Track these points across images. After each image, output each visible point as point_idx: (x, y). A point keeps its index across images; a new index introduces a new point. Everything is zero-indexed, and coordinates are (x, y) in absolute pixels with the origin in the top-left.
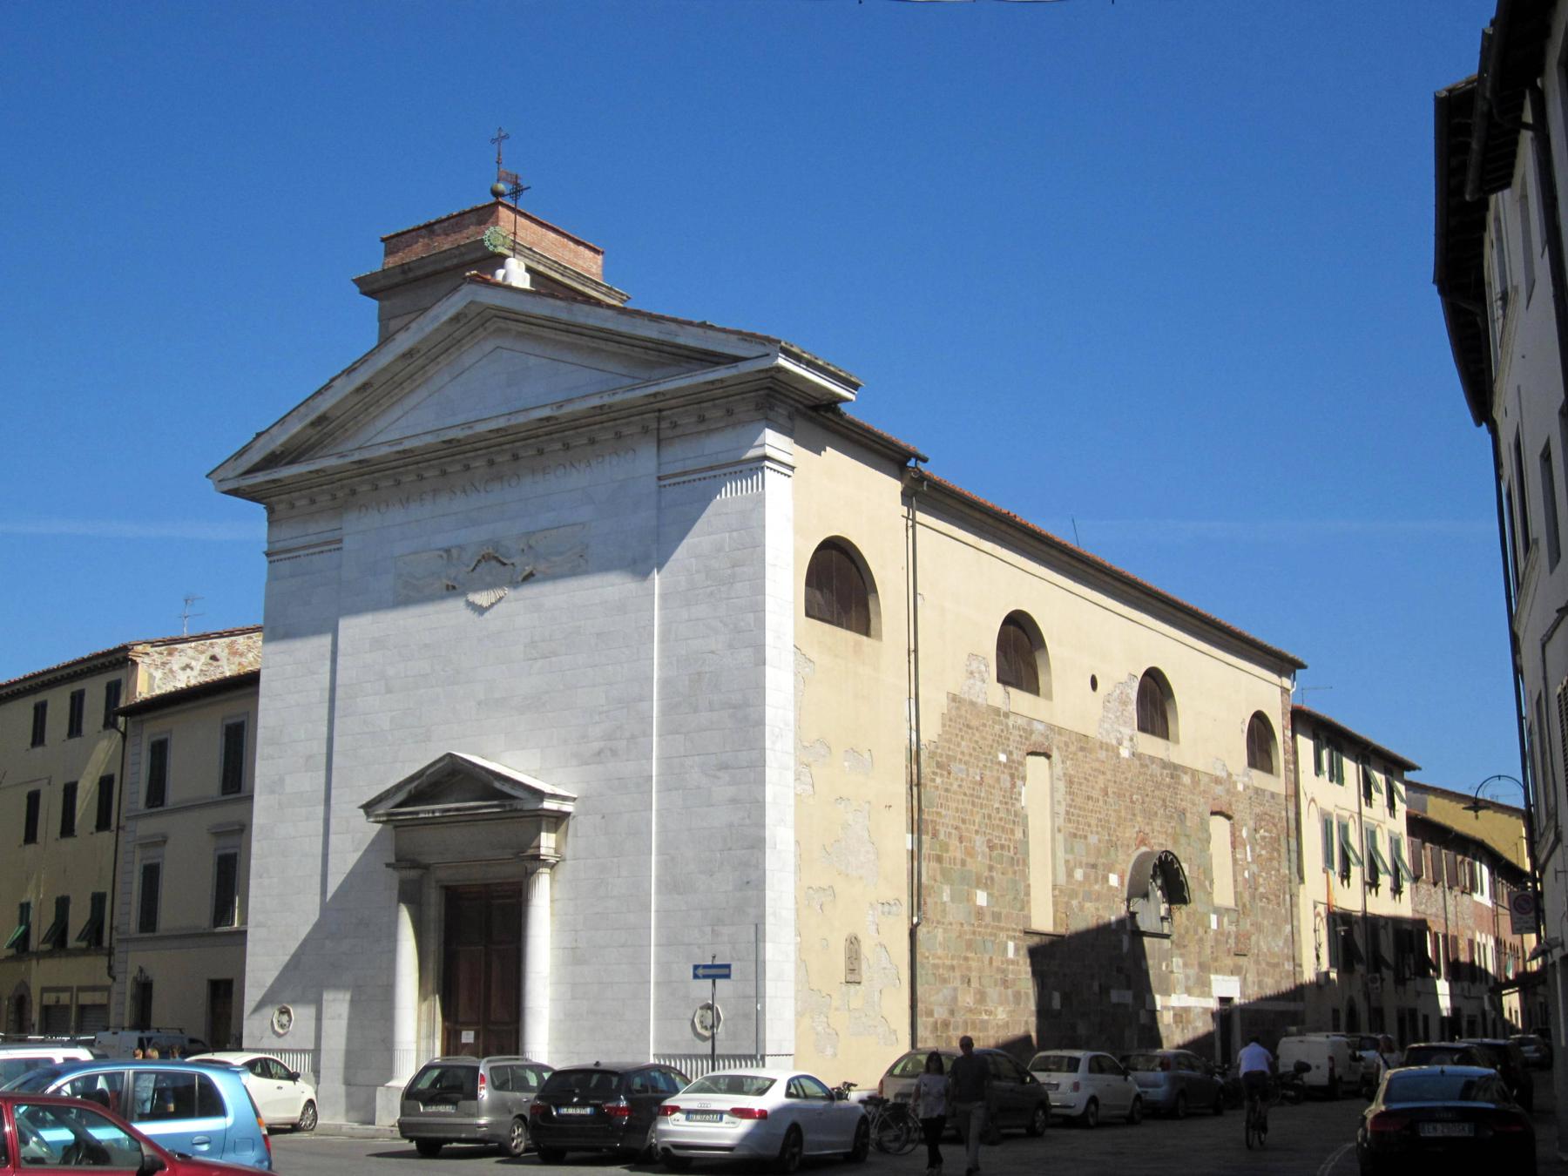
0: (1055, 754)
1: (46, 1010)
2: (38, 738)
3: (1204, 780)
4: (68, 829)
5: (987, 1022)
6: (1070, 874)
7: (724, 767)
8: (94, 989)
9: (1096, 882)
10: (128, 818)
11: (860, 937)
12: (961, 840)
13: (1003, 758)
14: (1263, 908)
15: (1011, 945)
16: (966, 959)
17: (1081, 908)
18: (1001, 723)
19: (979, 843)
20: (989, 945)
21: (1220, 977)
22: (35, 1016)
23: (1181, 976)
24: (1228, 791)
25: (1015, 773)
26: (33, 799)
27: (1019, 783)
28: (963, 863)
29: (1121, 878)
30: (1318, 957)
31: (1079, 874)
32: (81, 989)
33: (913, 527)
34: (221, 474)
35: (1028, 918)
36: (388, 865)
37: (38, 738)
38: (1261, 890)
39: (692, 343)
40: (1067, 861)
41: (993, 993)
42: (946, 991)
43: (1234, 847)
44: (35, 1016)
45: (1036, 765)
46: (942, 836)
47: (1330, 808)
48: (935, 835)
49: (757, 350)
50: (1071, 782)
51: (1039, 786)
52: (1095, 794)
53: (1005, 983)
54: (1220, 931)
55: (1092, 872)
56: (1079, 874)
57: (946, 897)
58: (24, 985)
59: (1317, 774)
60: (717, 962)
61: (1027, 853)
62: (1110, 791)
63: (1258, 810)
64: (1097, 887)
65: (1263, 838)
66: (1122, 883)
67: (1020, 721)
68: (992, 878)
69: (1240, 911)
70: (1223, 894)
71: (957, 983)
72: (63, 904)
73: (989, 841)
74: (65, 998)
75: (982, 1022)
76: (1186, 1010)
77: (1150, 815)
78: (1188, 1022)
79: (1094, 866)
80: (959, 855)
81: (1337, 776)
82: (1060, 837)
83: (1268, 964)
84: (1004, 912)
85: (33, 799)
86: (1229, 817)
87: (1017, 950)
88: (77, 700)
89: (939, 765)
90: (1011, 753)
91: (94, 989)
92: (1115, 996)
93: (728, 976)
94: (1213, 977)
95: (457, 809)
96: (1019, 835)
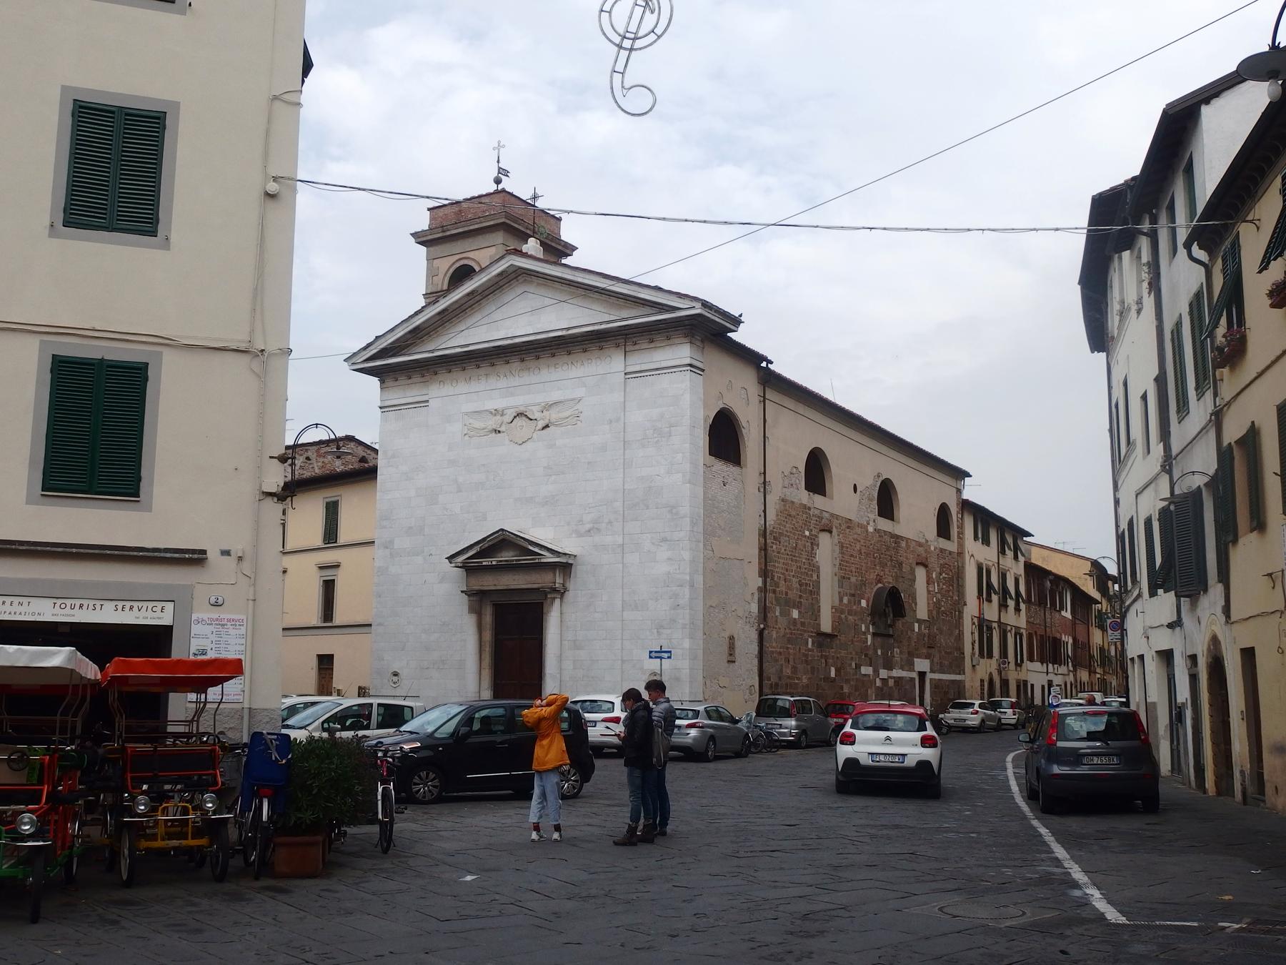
0: (834, 530)
7: (664, 540)
13: (807, 533)
25: (814, 543)
31: (845, 600)
45: (824, 539)
51: (826, 552)
56: (845, 600)
70: (922, 612)
77: (883, 565)
79: (853, 595)
81: (986, 542)
86: (926, 566)
96: (815, 577)
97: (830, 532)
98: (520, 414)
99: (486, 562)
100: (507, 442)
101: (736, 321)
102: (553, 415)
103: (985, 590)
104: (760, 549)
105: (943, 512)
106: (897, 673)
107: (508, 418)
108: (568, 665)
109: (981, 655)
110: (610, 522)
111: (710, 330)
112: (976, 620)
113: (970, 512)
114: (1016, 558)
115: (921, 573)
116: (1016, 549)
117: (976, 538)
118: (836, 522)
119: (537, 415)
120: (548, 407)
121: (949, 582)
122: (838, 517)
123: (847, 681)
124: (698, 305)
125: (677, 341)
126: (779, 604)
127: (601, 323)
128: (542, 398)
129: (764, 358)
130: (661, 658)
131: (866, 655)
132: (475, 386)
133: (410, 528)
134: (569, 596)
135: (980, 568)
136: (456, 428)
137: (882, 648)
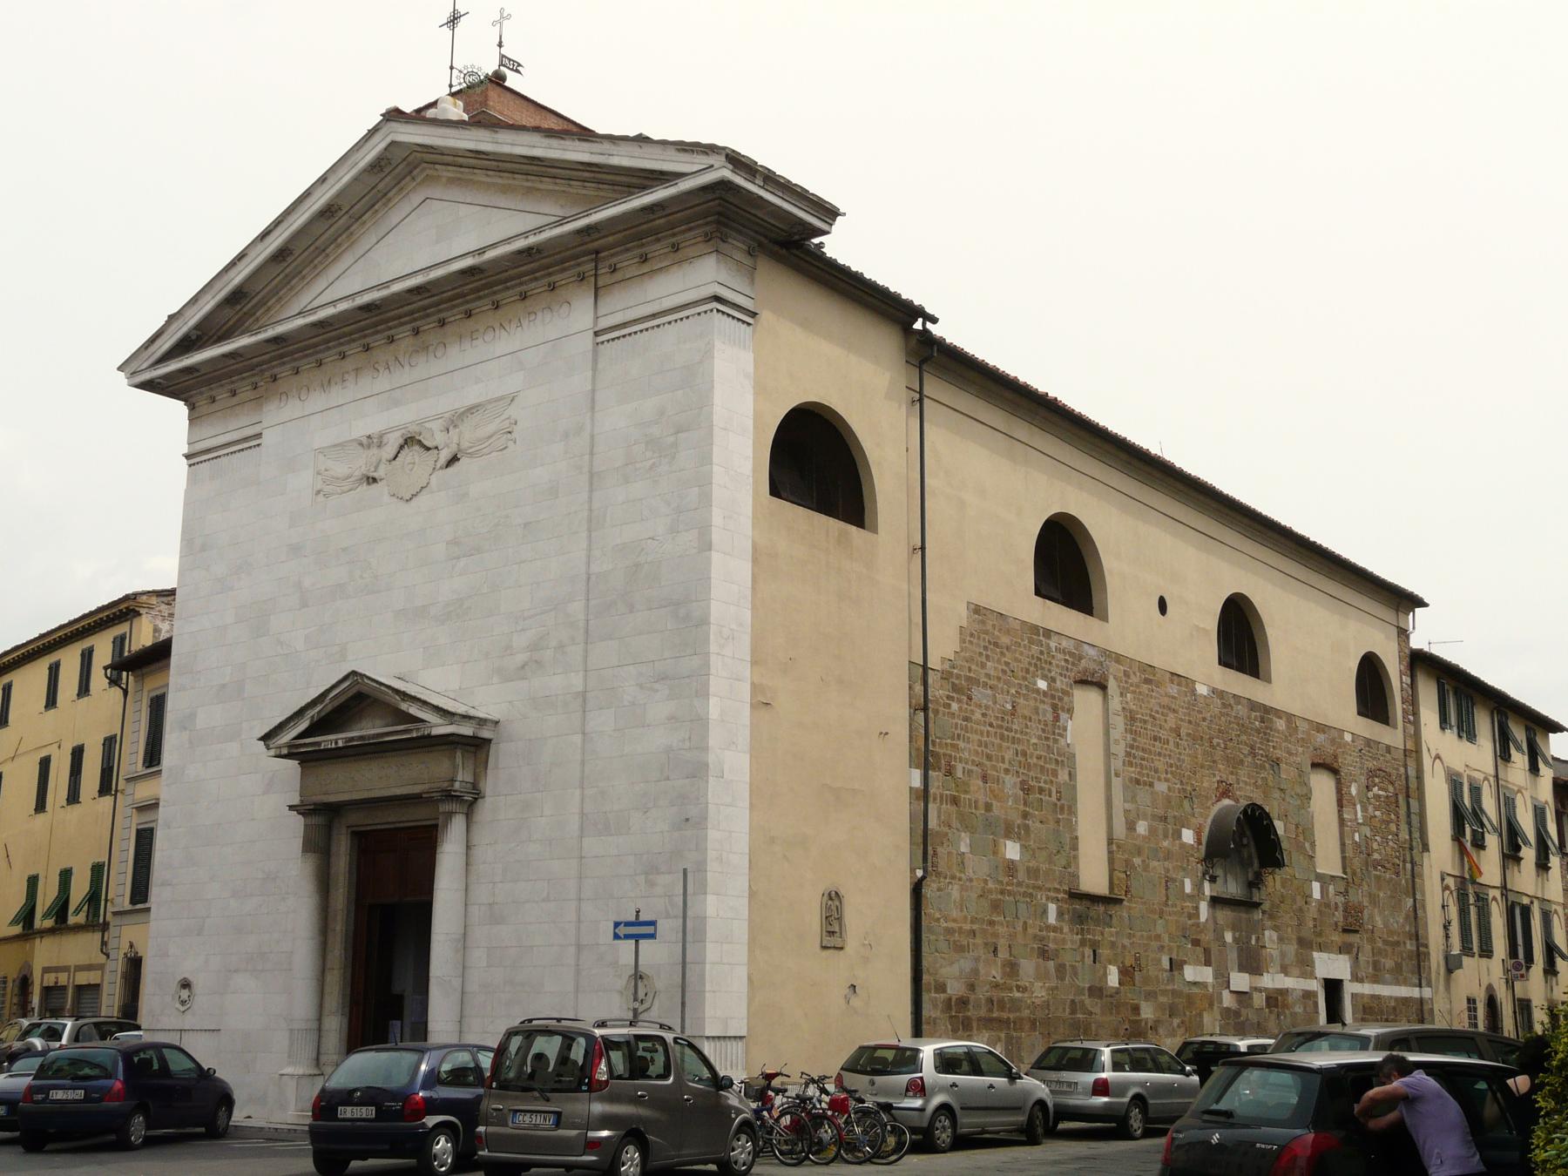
0: (1112, 685)
1: (47, 991)
2: (51, 702)
3: (1303, 726)
4: (73, 797)
5: (1020, 1000)
6: (1131, 827)
7: (663, 678)
8: (89, 968)
9: (1166, 837)
10: (128, 780)
11: (842, 892)
12: (985, 778)
13: (1042, 685)
14: (1378, 878)
15: (1052, 908)
16: (991, 923)
17: (1146, 868)
18: (1040, 643)
19: (1010, 782)
20: (1022, 907)
21: (1324, 955)
22: (36, 1000)
23: (1275, 953)
24: (1333, 741)
25: (1060, 706)
26: (45, 764)
27: (1064, 716)
28: (988, 807)
29: (1198, 834)
30: (1447, 937)
31: (1142, 828)
32: (79, 968)
33: (921, 400)
34: (134, 366)
35: (1075, 876)
36: (291, 807)
37: (51, 702)
38: (1376, 856)
39: (626, 162)
40: (1126, 811)
41: (1028, 966)
42: (965, 964)
43: (1340, 804)
44: (36, 1000)
45: (1086, 702)
46: (959, 774)
47: (1459, 767)
48: (950, 772)
49: (701, 161)
50: (1133, 719)
51: (1087, 724)
52: (1163, 734)
53: (1044, 954)
54: (1325, 904)
55: (1161, 826)
56: (1142, 828)
57: (964, 848)
58: (28, 966)
59: (1443, 729)
60: (642, 918)
61: (1074, 799)
62: (1183, 732)
63: (1371, 765)
64: (1165, 844)
65: (1377, 797)
66: (1199, 842)
67: (1064, 643)
68: (1027, 828)
69: (1348, 881)
70: (1328, 860)
71: (981, 952)
72: (66, 876)
73: (1023, 782)
74: (63, 979)
75: (1012, 1000)
76: (1284, 992)
77: (1234, 763)
78: (1285, 1006)
79: (1164, 819)
80: (982, 799)
81: (1467, 732)
82: (1117, 783)
83: (1385, 942)
84: (1043, 867)
85: (45, 764)
86: (1334, 771)
87: (1060, 914)
88: (87, 657)
89: (955, 688)
90: (1053, 680)
91: (89, 968)
92: (1191, 973)
93: (652, 936)
94: (1315, 954)
95: (361, 738)
96: (1063, 776)
97: (1103, 687)
98: (410, 441)
99: (329, 741)
100: (386, 498)
101: (830, 213)
102: (467, 434)
103: (1464, 818)
104: (914, 709)
105: (1370, 669)
106: (1272, 980)
107: (390, 450)
108: (478, 956)
109: (1467, 949)
110: (561, 647)
111: (761, 226)
112: (1450, 882)
113: (1429, 674)
114: (1534, 769)
115: (1322, 786)
116: (1534, 755)
117: (1444, 722)
118: (1114, 669)
119: (439, 439)
120: (454, 421)
121: (1390, 804)
122: (1119, 658)
123: (1150, 996)
124: (718, 160)
125: (691, 252)
126: (968, 828)
127: (539, 230)
128: (448, 403)
129: (919, 312)
130: (637, 938)
131: (1196, 943)
132: (337, 395)
133: (224, 686)
134: (485, 809)
135: (1455, 784)
136: (303, 481)
137: (1234, 928)
